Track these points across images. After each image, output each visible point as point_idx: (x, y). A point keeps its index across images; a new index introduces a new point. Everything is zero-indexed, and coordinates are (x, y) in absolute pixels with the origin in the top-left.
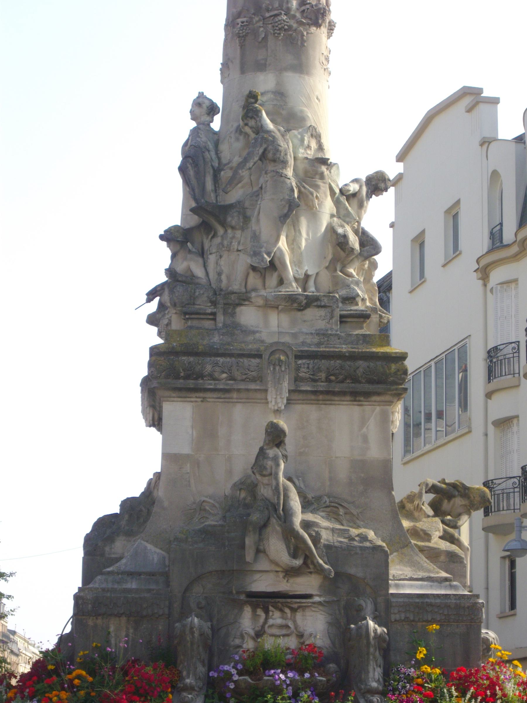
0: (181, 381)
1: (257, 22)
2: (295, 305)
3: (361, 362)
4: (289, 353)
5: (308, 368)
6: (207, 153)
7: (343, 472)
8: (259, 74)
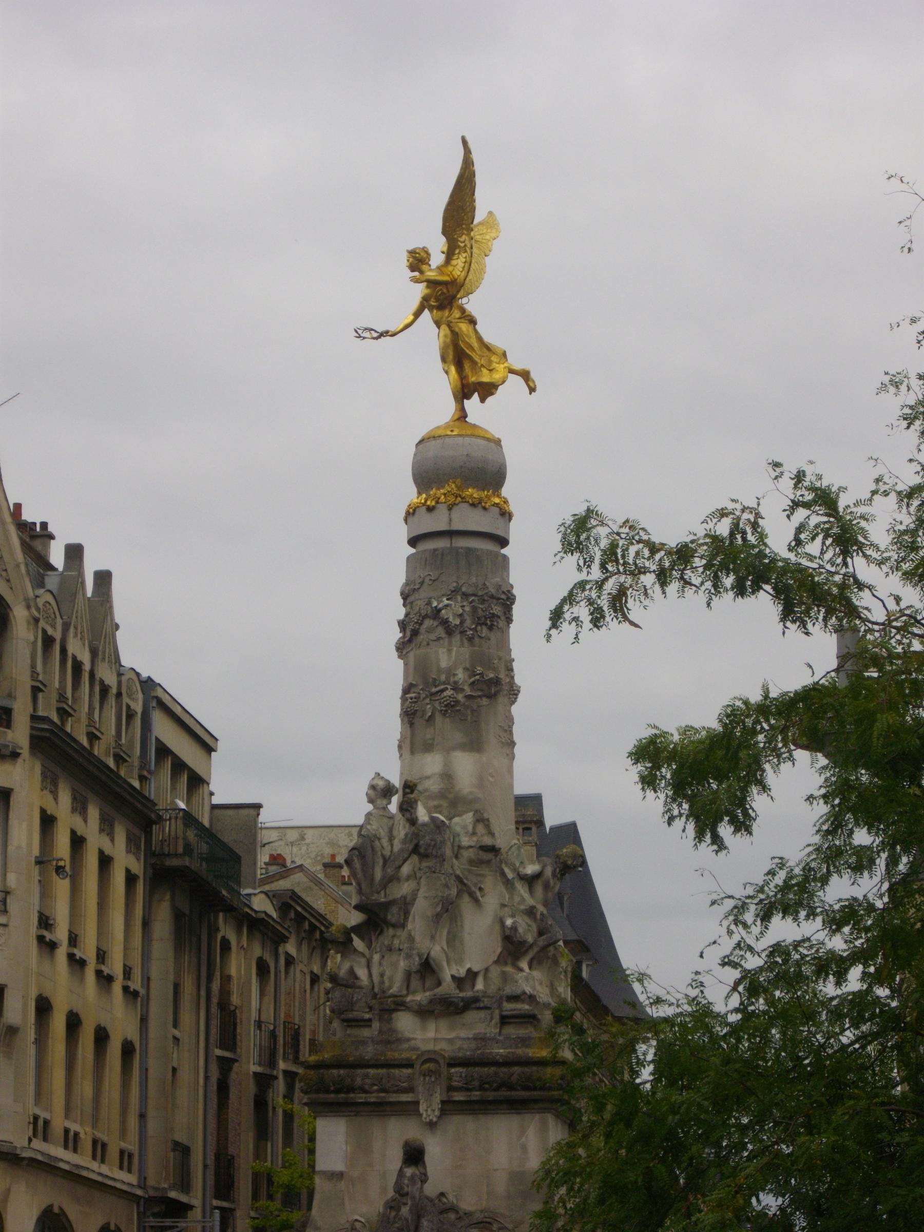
0: (332, 1096)
1: (424, 699)
2: (452, 1008)
3: (516, 1068)
4: (441, 1062)
5: (461, 1076)
6: (377, 842)
7: (501, 1185)
8: (426, 755)
